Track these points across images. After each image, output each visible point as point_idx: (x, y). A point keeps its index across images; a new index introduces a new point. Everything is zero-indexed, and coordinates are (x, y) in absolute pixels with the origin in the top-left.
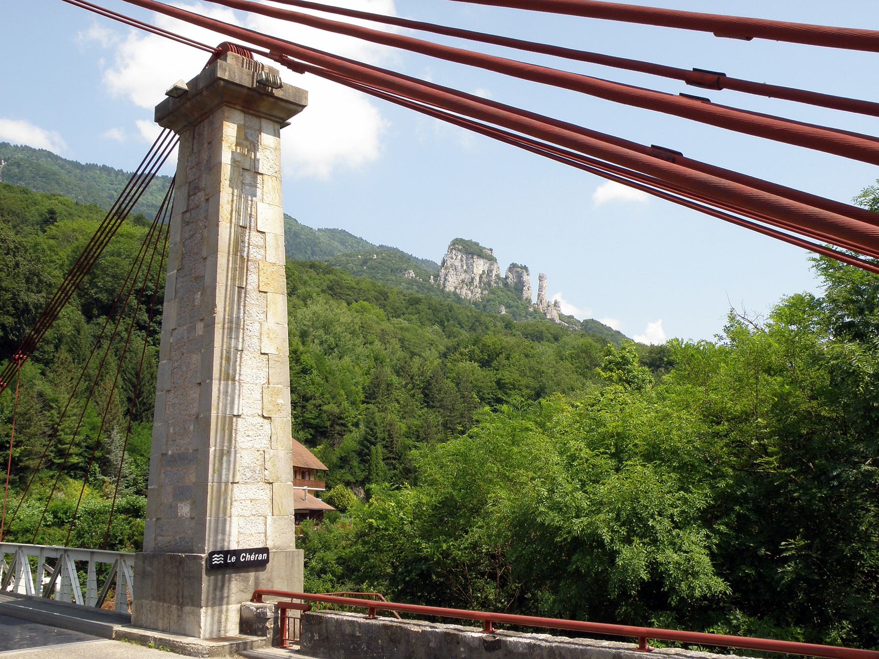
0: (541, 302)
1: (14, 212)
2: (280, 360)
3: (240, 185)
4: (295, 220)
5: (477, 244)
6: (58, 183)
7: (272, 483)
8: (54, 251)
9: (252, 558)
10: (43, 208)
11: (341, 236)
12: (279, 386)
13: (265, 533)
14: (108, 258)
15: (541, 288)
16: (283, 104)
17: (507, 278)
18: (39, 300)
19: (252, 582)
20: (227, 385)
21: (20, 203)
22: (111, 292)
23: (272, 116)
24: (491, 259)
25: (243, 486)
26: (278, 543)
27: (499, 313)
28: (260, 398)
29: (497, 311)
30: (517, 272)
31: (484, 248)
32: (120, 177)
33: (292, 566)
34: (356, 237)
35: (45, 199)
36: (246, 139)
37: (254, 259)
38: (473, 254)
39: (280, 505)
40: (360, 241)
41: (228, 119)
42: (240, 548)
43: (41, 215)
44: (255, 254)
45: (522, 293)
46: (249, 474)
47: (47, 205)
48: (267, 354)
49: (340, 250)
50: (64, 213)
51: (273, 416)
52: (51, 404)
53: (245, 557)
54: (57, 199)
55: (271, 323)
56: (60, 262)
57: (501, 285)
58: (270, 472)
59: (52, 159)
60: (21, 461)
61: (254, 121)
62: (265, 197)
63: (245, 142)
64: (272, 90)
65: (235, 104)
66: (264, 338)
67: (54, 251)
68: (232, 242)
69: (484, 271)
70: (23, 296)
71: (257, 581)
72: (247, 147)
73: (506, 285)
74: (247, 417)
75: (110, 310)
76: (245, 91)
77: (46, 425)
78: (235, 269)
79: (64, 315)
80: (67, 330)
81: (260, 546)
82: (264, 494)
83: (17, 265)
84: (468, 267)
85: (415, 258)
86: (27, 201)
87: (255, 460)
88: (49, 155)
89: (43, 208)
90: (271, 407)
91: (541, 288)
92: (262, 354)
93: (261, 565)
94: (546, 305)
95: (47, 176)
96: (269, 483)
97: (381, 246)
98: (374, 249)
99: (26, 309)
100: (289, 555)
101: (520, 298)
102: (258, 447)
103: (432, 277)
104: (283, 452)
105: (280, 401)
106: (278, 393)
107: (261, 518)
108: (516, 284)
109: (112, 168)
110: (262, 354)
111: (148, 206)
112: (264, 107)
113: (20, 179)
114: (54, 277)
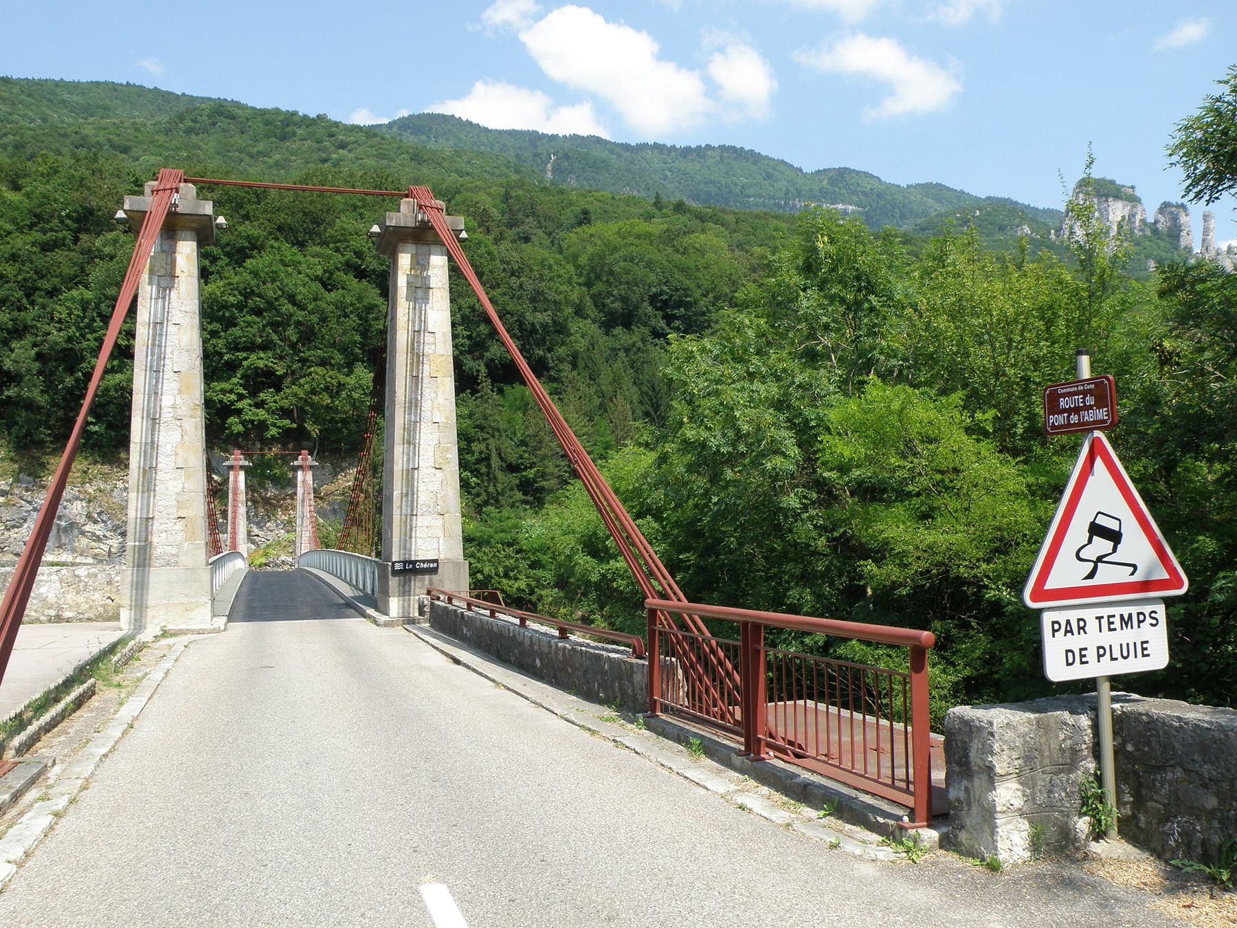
0: (1207, 249)
4: (878, 178)
5: (1112, 182)
6: (607, 171)
9: (425, 566)
11: (935, 191)
14: (622, 264)
15: (1206, 231)
17: (1156, 222)
19: (427, 582)
22: (624, 299)
24: (1133, 200)
27: (1146, 270)
29: (1143, 267)
30: (1171, 213)
31: (1123, 186)
32: (673, 154)
34: (955, 191)
36: (418, 263)
38: (1107, 196)
40: (961, 194)
41: (403, 252)
43: (576, 217)
45: (1179, 241)
47: (583, 204)
49: (936, 208)
50: (599, 211)
51: (443, 467)
55: (441, 399)
56: (567, 276)
57: (1148, 233)
60: (536, 482)
61: (424, 249)
66: (436, 412)
69: (1123, 217)
70: (529, 317)
73: (1155, 231)
75: (627, 319)
78: (412, 364)
80: (581, 345)
82: (438, 522)
83: (521, 286)
84: (1101, 214)
85: (1033, 208)
88: (598, 140)
90: (441, 461)
91: (1206, 231)
93: (434, 571)
94: (1213, 253)
95: (599, 166)
97: (989, 198)
98: (978, 203)
99: (534, 331)
100: (456, 564)
101: (1176, 248)
103: (1052, 231)
105: (449, 456)
106: (448, 450)
108: (1169, 229)
109: (664, 145)
111: (706, 183)
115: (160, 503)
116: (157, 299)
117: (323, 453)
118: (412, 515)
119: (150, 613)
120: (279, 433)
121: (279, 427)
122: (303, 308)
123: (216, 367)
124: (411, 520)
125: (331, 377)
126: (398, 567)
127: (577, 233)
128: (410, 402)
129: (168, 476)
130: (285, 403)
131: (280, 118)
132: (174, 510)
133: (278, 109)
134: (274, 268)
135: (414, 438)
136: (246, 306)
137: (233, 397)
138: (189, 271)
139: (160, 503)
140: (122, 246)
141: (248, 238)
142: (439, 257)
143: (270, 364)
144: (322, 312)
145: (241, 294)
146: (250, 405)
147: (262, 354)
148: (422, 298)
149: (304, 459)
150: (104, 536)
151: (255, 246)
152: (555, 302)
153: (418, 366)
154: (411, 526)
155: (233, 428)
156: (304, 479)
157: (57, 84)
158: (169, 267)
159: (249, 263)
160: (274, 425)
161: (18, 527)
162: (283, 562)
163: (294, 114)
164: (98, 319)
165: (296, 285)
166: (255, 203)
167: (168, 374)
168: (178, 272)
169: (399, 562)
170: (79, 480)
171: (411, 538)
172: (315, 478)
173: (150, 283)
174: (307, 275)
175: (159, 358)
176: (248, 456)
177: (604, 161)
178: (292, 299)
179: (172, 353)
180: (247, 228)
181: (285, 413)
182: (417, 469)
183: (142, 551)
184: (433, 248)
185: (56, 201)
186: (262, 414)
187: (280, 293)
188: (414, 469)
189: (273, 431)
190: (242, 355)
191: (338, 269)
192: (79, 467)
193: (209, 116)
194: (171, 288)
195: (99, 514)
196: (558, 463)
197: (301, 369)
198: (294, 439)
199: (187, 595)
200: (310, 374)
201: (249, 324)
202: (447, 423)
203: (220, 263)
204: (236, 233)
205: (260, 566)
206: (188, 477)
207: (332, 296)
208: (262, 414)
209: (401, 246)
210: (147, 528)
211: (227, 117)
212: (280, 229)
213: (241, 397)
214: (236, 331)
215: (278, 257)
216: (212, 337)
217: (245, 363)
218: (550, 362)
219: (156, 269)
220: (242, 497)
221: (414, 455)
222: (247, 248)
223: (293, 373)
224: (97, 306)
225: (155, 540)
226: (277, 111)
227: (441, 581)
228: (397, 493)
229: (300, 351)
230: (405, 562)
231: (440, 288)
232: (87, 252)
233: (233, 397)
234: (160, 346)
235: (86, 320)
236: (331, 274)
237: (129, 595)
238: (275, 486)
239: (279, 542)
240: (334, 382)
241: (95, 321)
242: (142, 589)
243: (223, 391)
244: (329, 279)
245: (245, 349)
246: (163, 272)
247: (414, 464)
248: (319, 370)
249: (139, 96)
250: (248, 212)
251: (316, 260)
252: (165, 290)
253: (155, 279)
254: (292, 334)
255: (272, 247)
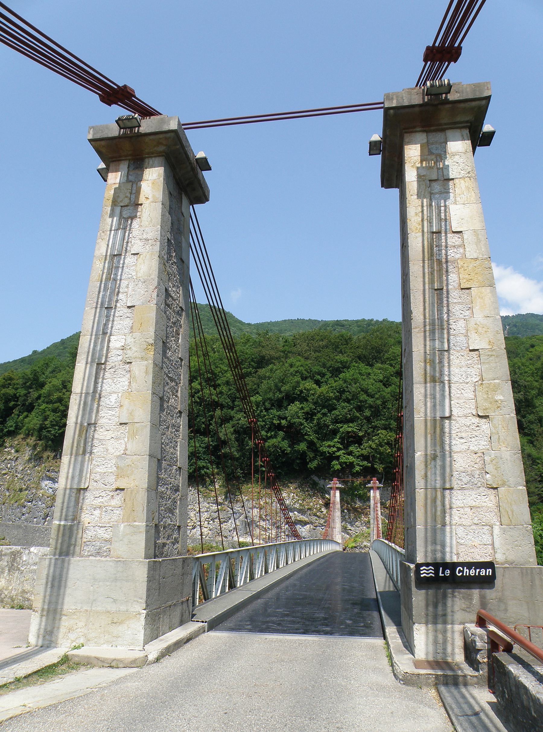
1: (511, 352)
2: (494, 353)
3: (428, 195)
7: (496, 488)
8: (526, 366)
9: (472, 572)
10: (527, 345)
12: (497, 381)
13: (493, 544)
16: (462, 105)
18: (519, 397)
20: (434, 388)
21: (514, 345)
23: (455, 123)
25: (459, 492)
26: (511, 558)
28: (473, 397)
33: (532, 586)
35: (528, 340)
36: (431, 153)
37: (452, 259)
39: (510, 513)
41: (409, 143)
42: (461, 560)
44: (453, 255)
46: (466, 479)
48: (477, 350)
51: (491, 414)
52: (537, 461)
53: (463, 572)
54: (535, 338)
58: (492, 475)
59: (534, 317)
61: (439, 136)
62: (458, 199)
63: (429, 157)
64: (446, 97)
65: (414, 127)
66: (473, 336)
67: (526, 366)
68: (426, 251)
71: (483, 604)
72: (432, 160)
74: (458, 419)
76: (417, 109)
77: (536, 475)
78: (432, 273)
79: (540, 404)
81: (488, 559)
86: (518, 343)
87: (472, 464)
89: (527, 345)
90: (487, 405)
92: (471, 351)
96: (495, 488)
102: (476, 449)
104: (508, 453)
105: (499, 397)
106: (496, 389)
107: (486, 528)
110: (471, 351)
112: (444, 117)
113: (518, 334)
114: (528, 381)
115: (98, 469)
116: (117, 230)
117: (388, 481)
118: (445, 489)
119: (65, 623)
120: (360, 469)
121: (361, 466)
122: (372, 396)
123: (326, 434)
124: (443, 497)
125: (389, 436)
126: (425, 572)
127: (531, 352)
128: (433, 324)
129: (109, 435)
130: (365, 452)
131: (366, 323)
132: (112, 479)
133: (364, 319)
134: (355, 377)
135: (442, 374)
136: (341, 398)
137: (335, 449)
138: (154, 196)
139: (98, 469)
140: (275, 372)
141: (341, 362)
142: (460, 143)
143: (355, 430)
144: (384, 397)
145: (338, 392)
146: (344, 454)
147: (351, 425)
148: (441, 193)
149: (374, 483)
150: (268, 528)
151: (345, 366)
152: (525, 386)
153: (440, 277)
154: (443, 505)
155: (335, 467)
156: (375, 495)
157: (269, 323)
158: (133, 196)
159: (342, 376)
160: (358, 465)
161: (226, 522)
162: (365, 546)
163: (372, 320)
164: (264, 411)
165: (368, 384)
166: (345, 344)
167: (121, 310)
168: (142, 200)
169: (427, 565)
170: (256, 497)
171: (444, 525)
172: (381, 495)
173: (112, 215)
174: (374, 380)
175: (112, 293)
176: (344, 482)
177: (537, 325)
178: (366, 391)
179: (127, 287)
180: (340, 357)
181: (365, 458)
182: (449, 418)
183: (67, 532)
184: (449, 133)
185: (246, 354)
186: (351, 459)
187: (359, 389)
188: (443, 418)
189: (357, 468)
190: (339, 425)
191: (392, 376)
192: (256, 490)
193: (332, 326)
194: (133, 218)
195: (266, 516)
196: (537, 486)
197: (373, 432)
198: (369, 472)
199: (115, 601)
200: (378, 434)
201: (343, 408)
202: (492, 350)
203: (327, 377)
204: (335, 360)
205: (352, 548)
206: (133, 435)
207: (389, 389)
208: (351, 459)
209: (407, 138)
210: (77, 502)
211: (341, 326)
212: (360, 358)
213: (339, 449)
214: (336, 412)
215: (357, 371)
216: (323, 416)
217: (341, 430)
218: (525, 424)
219: (119, 200)
220: (338, 506)
221: (443, 396)
222: (341, 368)
223: (369, 434)
224: (264, 404)
225: (85, 518)
226: (364, 320)
227: (500, 600)
228: (419, 455)
229: (372, 422)
230: (436, 566)
231: (463, 178)
232: (260, 377)
233: (335, 449)
234: (115, 280)
235: (258, 412)
236: (388, 378)
237: (42, 594)
238: (360, 501)
239: (363, 534)
240: (392, 439)
241: (262, 412)
242: (59, 587)
243: (329, 446)
244: (387, 381)
245: (340, 422)
246: (126, 201)
247: (443, 411)
248: (383, 432)
249: (303, 323)
250: (341, 350)
251: (379, 371)
252: (126, 219)
253: (118, 210)
254: (367, 413)
255: (354, 366)
